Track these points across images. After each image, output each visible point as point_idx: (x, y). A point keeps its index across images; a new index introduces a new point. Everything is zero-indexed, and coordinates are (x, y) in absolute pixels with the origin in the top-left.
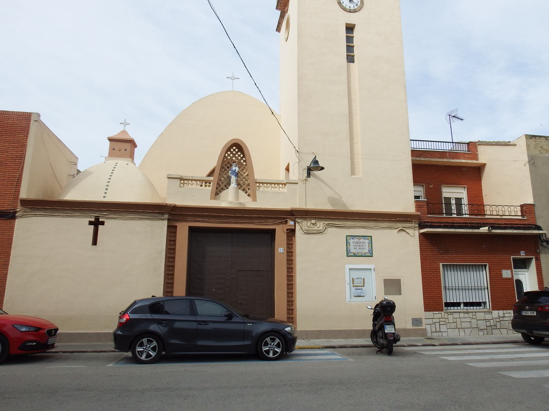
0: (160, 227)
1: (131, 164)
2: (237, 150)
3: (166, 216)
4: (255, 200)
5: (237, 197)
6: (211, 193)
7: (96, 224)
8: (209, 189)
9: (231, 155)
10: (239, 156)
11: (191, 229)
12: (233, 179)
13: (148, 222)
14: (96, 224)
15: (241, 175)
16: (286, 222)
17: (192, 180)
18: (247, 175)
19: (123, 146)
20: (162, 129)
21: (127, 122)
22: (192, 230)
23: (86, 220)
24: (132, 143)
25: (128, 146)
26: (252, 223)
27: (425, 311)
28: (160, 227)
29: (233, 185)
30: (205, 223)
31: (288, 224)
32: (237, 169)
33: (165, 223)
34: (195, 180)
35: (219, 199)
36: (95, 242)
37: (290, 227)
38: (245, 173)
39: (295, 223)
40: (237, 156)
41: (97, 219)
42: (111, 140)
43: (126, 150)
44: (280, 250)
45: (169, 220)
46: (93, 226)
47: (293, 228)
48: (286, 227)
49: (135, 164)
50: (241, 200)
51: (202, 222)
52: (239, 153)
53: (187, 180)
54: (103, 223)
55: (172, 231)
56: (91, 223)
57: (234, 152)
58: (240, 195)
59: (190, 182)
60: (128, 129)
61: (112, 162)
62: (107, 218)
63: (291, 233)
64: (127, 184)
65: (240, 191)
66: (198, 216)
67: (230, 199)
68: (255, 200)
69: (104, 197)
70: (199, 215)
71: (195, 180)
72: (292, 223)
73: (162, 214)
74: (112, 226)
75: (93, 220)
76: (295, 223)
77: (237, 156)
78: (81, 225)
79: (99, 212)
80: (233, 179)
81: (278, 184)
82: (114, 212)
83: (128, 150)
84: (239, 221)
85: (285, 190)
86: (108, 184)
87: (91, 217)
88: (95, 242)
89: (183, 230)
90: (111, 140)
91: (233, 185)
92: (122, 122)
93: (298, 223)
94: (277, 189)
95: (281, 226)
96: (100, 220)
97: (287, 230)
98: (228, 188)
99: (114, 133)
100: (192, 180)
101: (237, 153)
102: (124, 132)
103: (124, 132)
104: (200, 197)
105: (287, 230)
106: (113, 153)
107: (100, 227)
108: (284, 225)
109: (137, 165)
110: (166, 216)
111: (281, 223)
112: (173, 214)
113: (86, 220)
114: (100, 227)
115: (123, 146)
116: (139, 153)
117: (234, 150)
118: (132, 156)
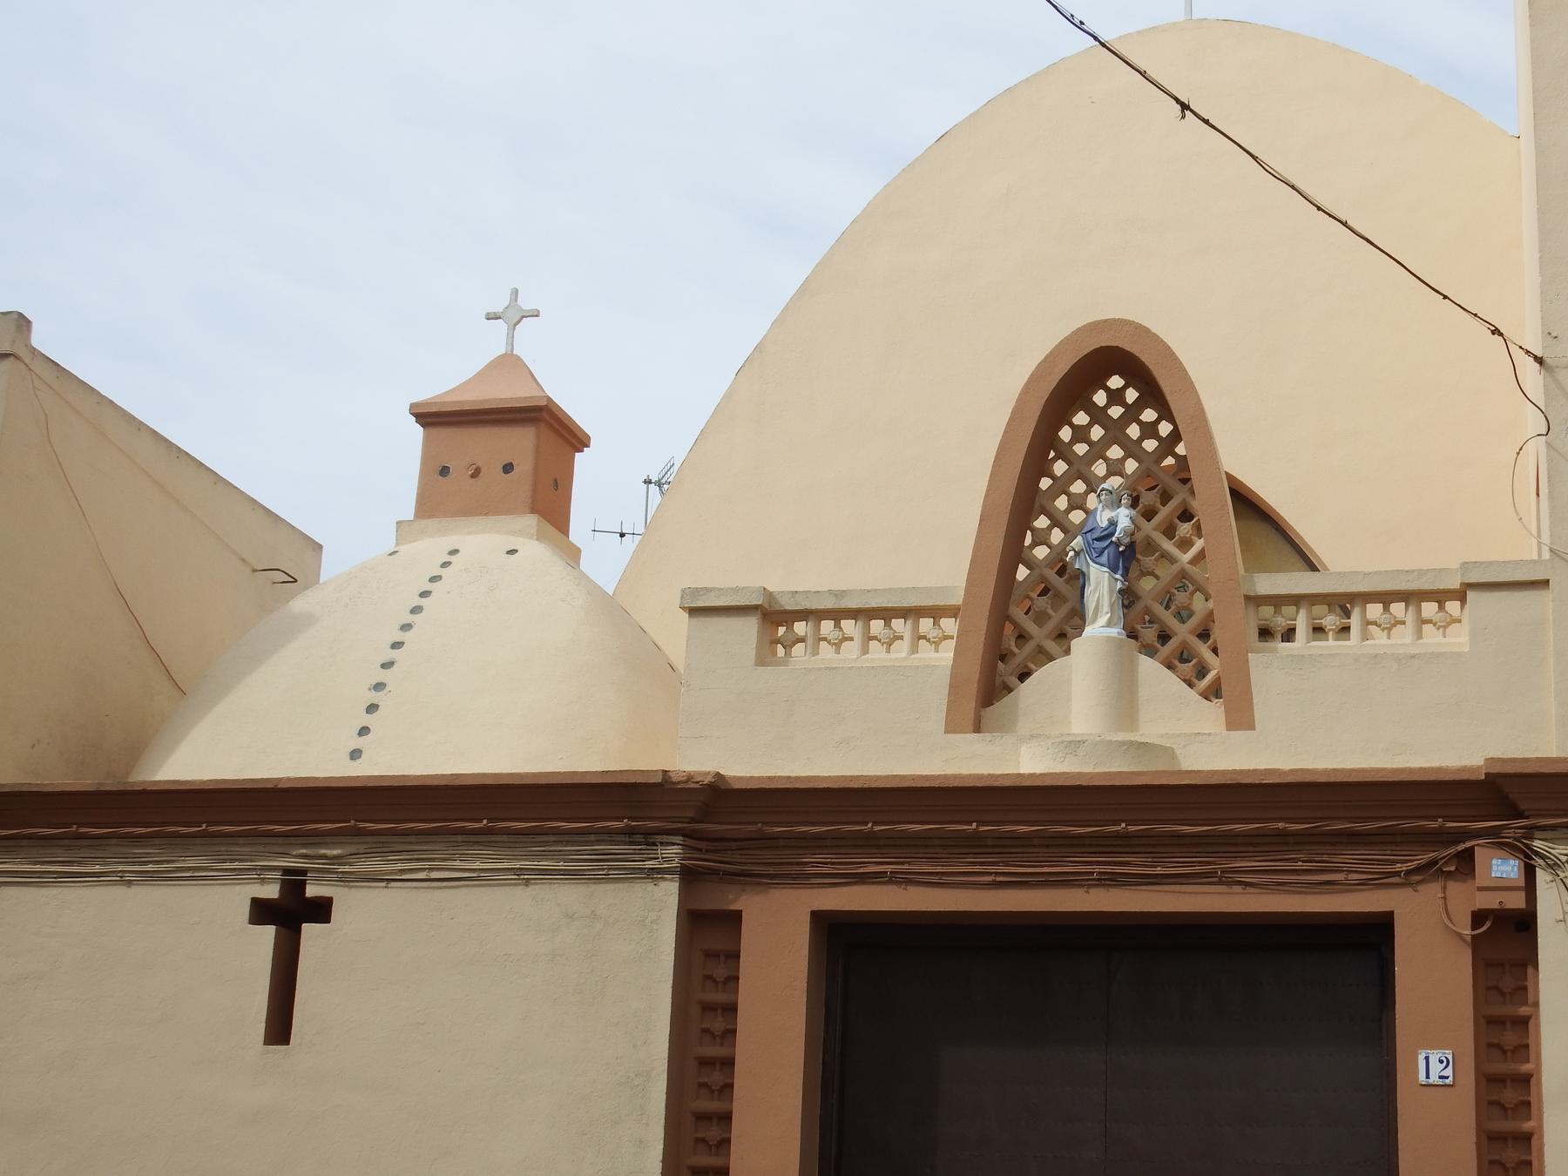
0: (637, 923)
1: (535, 551)
2: (1131, 395)
3: (672, 853)
4: (1241, 718)
5: (1124, 700)
6: (955, 687)
7: (290, 913)
8: (938, 657)
9: (1097, 433)
10: (1150, 430)
11: (828, 927)
12: (1101, 584)
13: (569, 895)
14: (290, 913)
15: (1165, 556)
16: (1466, 863)
17: (837, 615)
18: (1201, 555)
19: (504, 448)
20: (755, 328)
21: (526, 303)
22: (837, 937)
23: (236, 897)
24: (556, 433)
25: (520, 443)
26: (1225, 879)
27: (813, 913)
28: (637, 923)
29: (1101, 626)
30: (914, 891)
31: (1480, 880)
32: (1124, 517)
33: (668, 893)
34: (854, 614)
35: (1005, 727)
36: (279, 1028)
37: (1490, 901)
38: (1185, 544)
39: (1530, 872)
40: (1134, 431)
41: (294, 882)
42: (430, 418)
43: (508, 468)
44: (1433, 1065)
45: (690, 877)
46: (270, 931)
47: (1517, 901)
48: (1464, 899)
49: (572, 555)
50: (1149, 731)
51: (892, 879)
52: (1100, 398)
53: (804, 615)
54: (321, 911)
55: (708, 944)
56: (262, 912)
57: (1116, 412)
58: (1144, 692)
59: (827, 626)
60: (532, 345)
61: (431, 546)
62: (346, 880)
63: (1507, 940)
64: (486, 669)
65: (1150, 669)
66: (871, 843)
67: (1085, 717)
68: (1241, 718)
69: (355, 754)
70: (872, 836)
71: (854, 614)
72: (1505, 868)
73: (648, 839)
74: (378, 924)
75: (271, 891)
76: (1530, 872)
77: (1116, 412)
78: (206, 923)
79: (307, 842)
80: (1101, 584)
81: (1411, 597)
82: (382, 843)
83: (524, 467)
84: (1135, 865)
85: (1456, 636)
86: (384, 675)
87: (260, 875)
88: (279, 1028)
89: (777, 941)
90: (430, 418)
91: (1101, 626)
92: (499, 309)
93: (1554, 866)
94: (1403, 637)
95: (1432, 890)
96: (312, 891)
97: (1478, 917)
98: (1068, 652)
99: (449, 375)
100: (837, 615)
101: (1132, 413)
102: (509, 363)
103: (509, 363)
104: (881, 721)
105: (1478, 917)
106: (444, 493)
107: (308, 929)
108: (1454, 887)
109: (605, 562)
110: (672, 853)
111: (1429, 871)
112: (711, 836)
113: (236, 897)
114: (308, 929)
115: (504, 448)
116: (601, 487)
117: (1116, 397)
118: (550, 504)
